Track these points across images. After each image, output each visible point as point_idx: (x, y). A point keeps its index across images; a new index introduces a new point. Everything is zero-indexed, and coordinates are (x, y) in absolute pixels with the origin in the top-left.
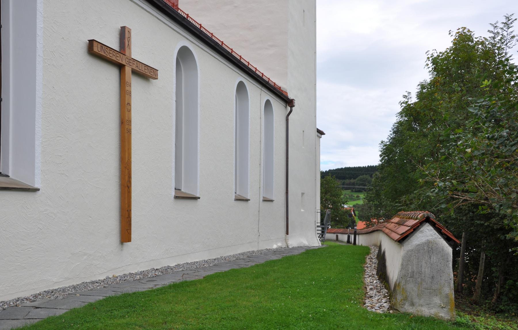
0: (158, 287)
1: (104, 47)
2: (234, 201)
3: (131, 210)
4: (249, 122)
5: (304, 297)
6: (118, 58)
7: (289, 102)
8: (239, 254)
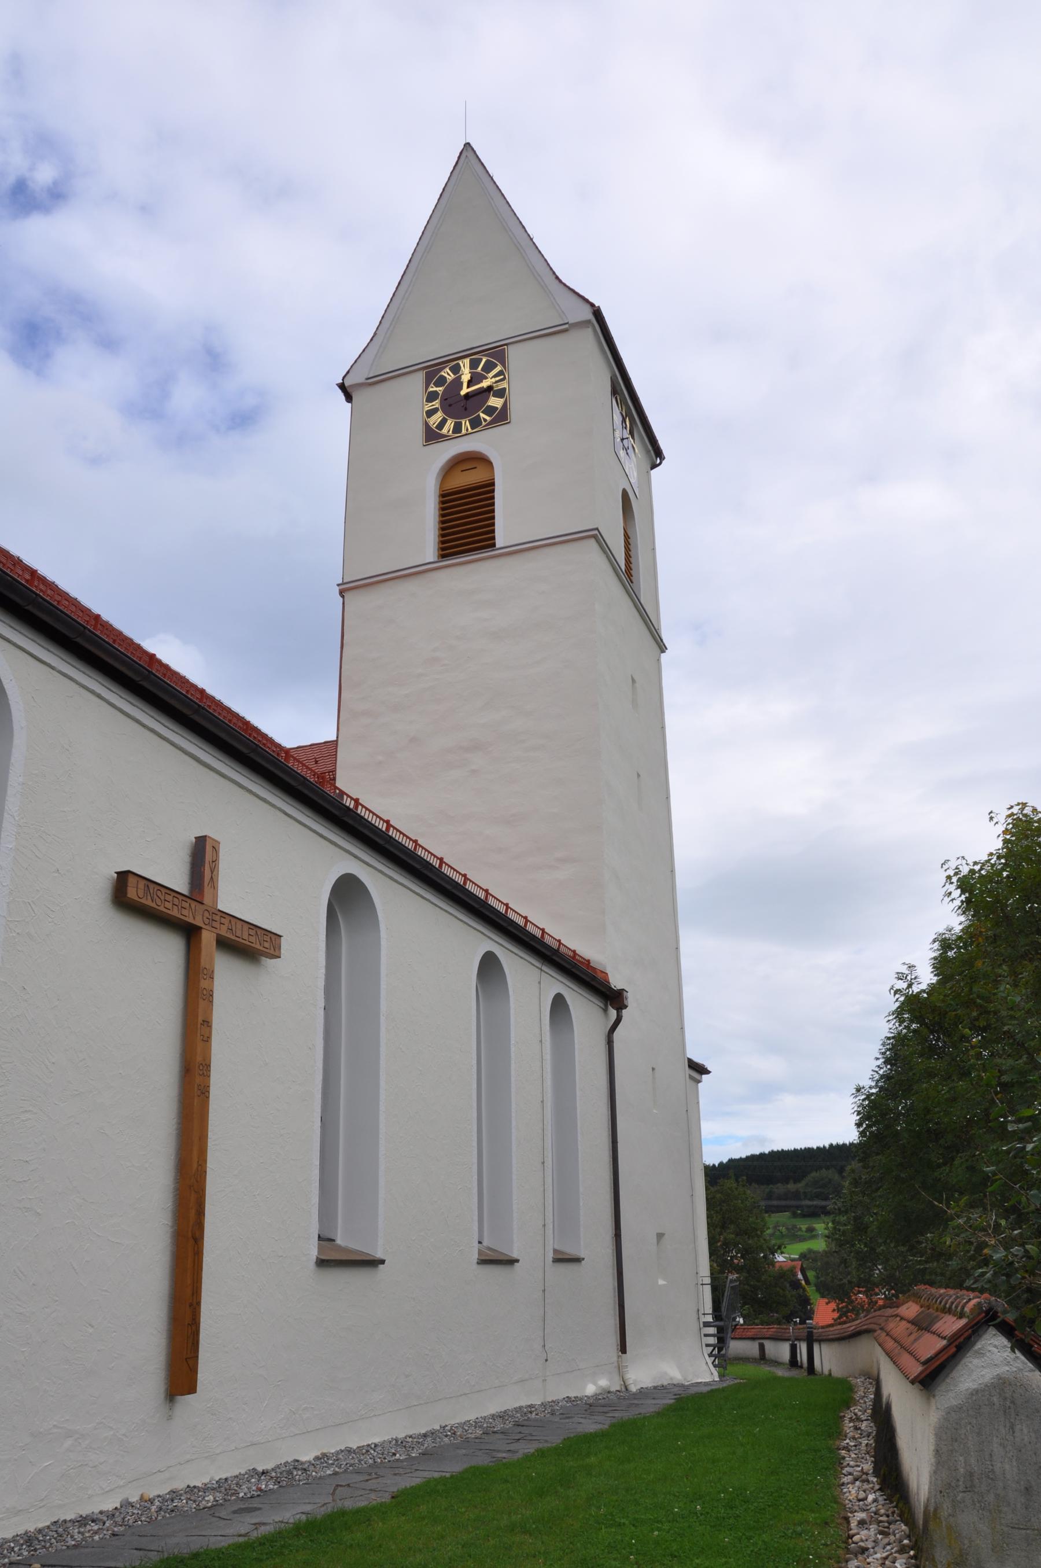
0: (263, 1530)
1: (151, 886)
2: (475, 1266)
3: (199, 1303)
4: (513, 1055)
5: (673, 1556)
6: (185, 912)
7: (613, 999)
8: (493, 1416)
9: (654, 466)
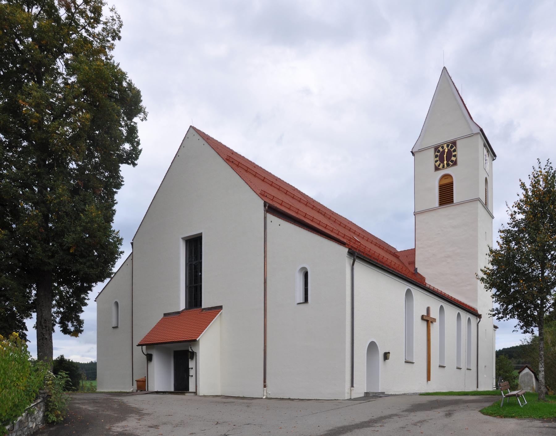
9: (494, 160)
